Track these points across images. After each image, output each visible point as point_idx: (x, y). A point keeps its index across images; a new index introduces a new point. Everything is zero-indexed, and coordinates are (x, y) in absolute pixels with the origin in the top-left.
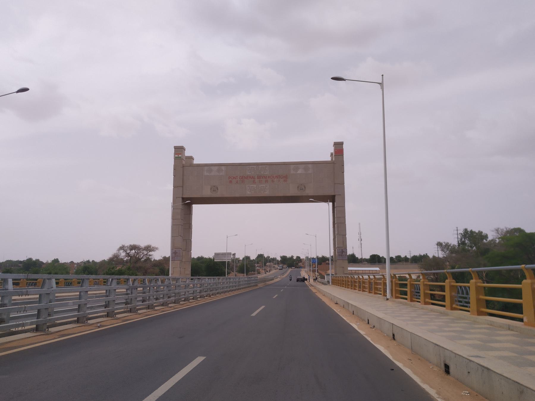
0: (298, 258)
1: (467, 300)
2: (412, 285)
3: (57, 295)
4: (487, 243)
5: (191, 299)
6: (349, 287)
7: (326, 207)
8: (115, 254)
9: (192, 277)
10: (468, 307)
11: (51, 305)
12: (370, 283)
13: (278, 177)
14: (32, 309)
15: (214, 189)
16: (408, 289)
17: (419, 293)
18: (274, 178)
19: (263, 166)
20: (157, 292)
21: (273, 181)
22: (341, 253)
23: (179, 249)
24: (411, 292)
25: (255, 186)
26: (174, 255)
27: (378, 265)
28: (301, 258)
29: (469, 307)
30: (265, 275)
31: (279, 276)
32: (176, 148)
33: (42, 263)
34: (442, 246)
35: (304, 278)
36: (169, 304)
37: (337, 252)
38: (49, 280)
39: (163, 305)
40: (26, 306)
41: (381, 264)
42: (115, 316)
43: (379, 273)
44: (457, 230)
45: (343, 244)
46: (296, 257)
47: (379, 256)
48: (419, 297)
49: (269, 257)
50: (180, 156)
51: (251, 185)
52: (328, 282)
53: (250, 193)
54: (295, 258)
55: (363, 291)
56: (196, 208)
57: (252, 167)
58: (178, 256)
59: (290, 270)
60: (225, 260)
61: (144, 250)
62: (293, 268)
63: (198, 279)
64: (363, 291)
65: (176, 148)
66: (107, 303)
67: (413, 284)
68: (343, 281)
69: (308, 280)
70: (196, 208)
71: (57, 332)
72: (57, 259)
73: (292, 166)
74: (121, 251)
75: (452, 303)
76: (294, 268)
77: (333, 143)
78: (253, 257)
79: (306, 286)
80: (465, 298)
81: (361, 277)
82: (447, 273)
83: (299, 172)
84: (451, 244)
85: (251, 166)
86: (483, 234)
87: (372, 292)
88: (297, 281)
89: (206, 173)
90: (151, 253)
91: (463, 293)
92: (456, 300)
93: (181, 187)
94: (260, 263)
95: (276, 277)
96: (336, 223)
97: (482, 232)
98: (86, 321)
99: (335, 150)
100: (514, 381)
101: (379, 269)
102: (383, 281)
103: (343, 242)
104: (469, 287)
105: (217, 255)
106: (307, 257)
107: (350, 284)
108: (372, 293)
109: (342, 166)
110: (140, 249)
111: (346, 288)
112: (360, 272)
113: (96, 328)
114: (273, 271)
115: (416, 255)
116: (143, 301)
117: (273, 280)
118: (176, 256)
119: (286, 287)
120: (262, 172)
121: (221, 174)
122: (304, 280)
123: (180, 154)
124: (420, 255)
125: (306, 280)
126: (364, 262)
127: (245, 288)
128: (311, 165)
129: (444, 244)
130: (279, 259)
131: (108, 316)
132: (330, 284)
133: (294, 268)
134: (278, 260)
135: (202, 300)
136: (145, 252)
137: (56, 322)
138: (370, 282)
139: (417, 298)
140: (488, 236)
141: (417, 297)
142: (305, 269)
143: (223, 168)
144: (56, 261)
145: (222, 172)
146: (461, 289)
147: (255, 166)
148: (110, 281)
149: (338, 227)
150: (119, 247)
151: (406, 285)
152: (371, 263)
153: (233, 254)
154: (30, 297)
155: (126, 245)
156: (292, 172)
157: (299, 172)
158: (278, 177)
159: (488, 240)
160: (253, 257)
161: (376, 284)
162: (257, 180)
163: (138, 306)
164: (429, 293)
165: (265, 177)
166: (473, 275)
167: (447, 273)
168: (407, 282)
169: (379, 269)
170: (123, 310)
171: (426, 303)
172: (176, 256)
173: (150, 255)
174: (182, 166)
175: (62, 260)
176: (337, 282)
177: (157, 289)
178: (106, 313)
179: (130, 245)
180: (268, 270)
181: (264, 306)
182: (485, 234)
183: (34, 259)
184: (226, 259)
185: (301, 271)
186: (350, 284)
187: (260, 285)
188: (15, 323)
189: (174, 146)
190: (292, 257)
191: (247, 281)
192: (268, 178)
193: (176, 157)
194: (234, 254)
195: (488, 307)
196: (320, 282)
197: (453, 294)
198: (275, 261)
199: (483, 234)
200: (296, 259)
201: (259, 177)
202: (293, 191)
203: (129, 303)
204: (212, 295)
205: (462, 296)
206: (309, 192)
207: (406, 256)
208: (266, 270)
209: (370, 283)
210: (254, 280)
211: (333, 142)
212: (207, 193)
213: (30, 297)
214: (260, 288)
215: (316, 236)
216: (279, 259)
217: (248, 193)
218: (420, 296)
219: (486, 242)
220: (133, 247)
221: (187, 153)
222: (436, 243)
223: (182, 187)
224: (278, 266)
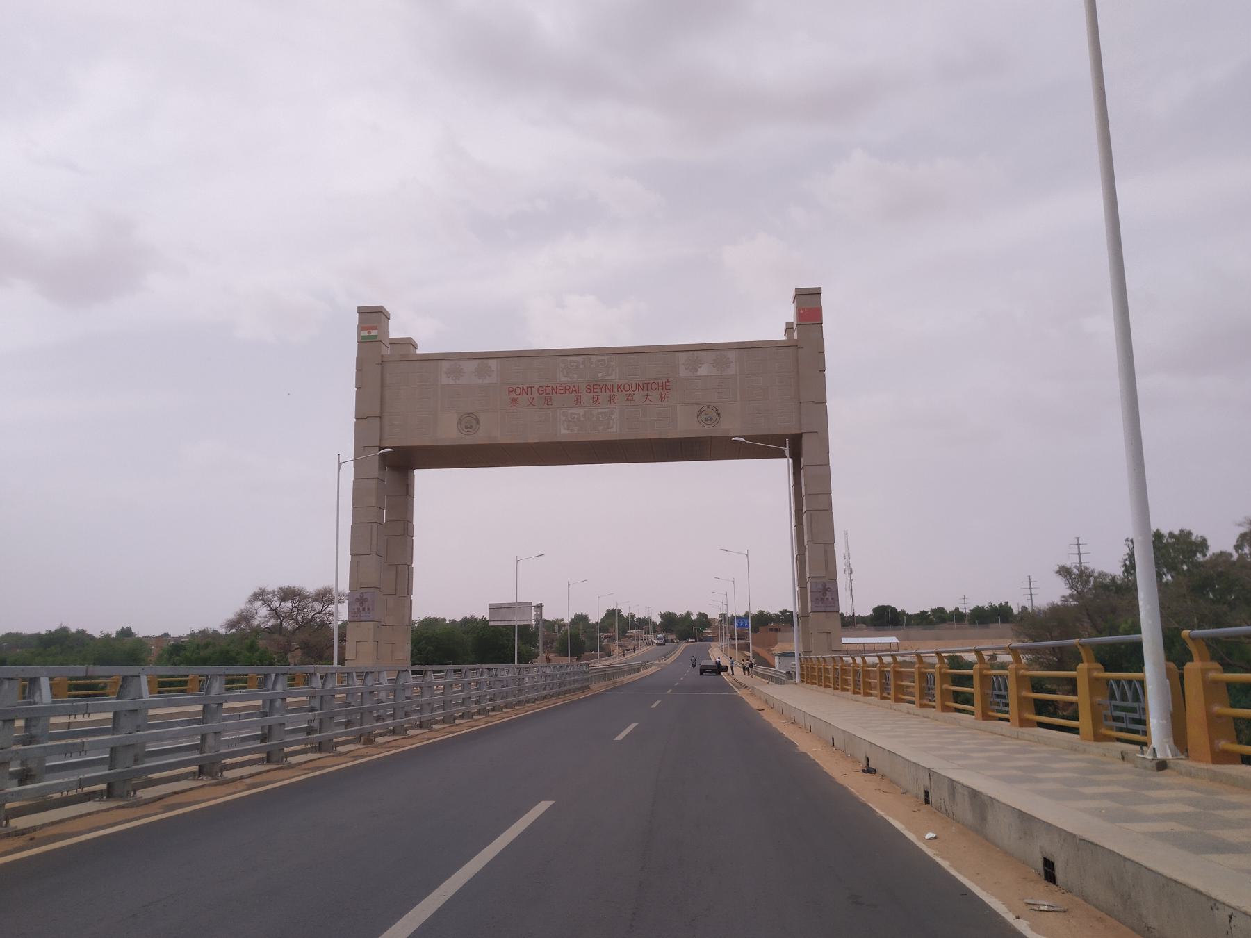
0: (703, 616)
1: (1136, 716)
2: (984, 677)
3: (151, 712)
4: (1206, 562)
5: (438, 722)
6: (814, 681)
7: (780, 468)
8: (241, 610)
9: (417, 668)
10: (1141, 732)
11: (226, 725)
12: (883, 674)
13: (645, 385)
14: (95, 747)
15: (469, 421)
16: (975, 690)
17: (1004, 697)
18: (634, 389)
19: (603, 357)
20: (28, 740)
21: (630, 398)
22: (821, 593)
23: (372, 590)
24: (984, 695)
25: (581, 412)
26: (357, 606)
27: (895, 630)
28: (709, 618)
29: (934, 701)
30: (622, 658)
31: (657, 662)
32: (362, 312)
33: (91, 637)
34: (1071, 576)
35: (718, 663)
36: (488, 711)
37: (811, 592)
38: (12, 681)
39: (393, 732)
40: (85, 740)
41: (902, 627)
42: (284, 759)
43: (898, 651)
44: (1078, 545)
45: (827, 568)
46: (698, 615)
47: (894, 610)
48: (1006, 709)
49: (633, 616)
50: (374, 333)
51: (570, 411)
52: (790, 675)
53: (566, 432)
54: (694, 617)
55: (825, 687)
56: (424, 479)
57: (571, 361)
58: (369, 609)
59: (684, 645)
60: (512, 623)
61: (316, 600)
62: (690, 640)
63: (455, 671)
64: (866, 694)
65: (362, 312)
66: (266, 731)
67: (986, 676)
68: (827, 670)
69: (729, 671)
70: (424, 479)
71: (250, 777)
72: (129, 629)
73: (682, 357)
74: (258, 604)
75: (1096, 722)
76: (694, 640)
77: (792, 293)
78: (595, 617)
79: (725, 687)
80: (1133, 710)
81: (859, 660)
82: (1079, 646)
83: (703, 371)
84: (1093, 572)
85: (569, 359)
86: (1193, 538)
87: (933, 704)
88: (701, 674)
89: (445, 380)
90: (331, 608)
91: (1124, 698)
92: (1105, 716)
93: (378, 419)
94: (611, 630)
95: (646, 663)
96: (804, 510)
97: (1190, 534)
98: (132, 793)
99: (798, 310)
100: (1014, 808)
101: (898, 641)
102: (919, 668)
103: (826, 562)
104: (1007, 676)
105: (494, 608)
106: (724, 616)
107: (816, 674)
108: (889, 699)
109: (820, 352)
110: (306, 597)
111: (837, 689)
112: (851, 647)
113: (310, 771)
114: (644, 649)
115: (980, 605)
116: (347, 724)
117: (638, 670)
118: (364, 609)
119: (669, 692)
120: (600, 375)
121: (486, 381)
122: (718, 669)
123: (375, 328)
124: (991, 606)
125: (725, 669)
126: (858, 625)
127: (574, 690)
128: (733, 352)
129: (1075, 571)
130: (657, 620)
131: (268, 760)
132: (798, 680)
133: (694, 640)
134: (654, 623)
135: (466, 725)
136: (318, 606)
137: (52, 797)
138: (856, 670)
139: (998, 711)
140: (1209, 543)
141: (1119, 724)
142: (721, 644)
143: (493, 364)
144: (126, 633)
145: (489, 376)
146: (1118, 686)
147: (580, 359)
148: (273, 678)
149: (811, 522)
150: (253, 593)
151: (970, 677)
152: (875, 625)
153: (537, 607)
154: (94, 717)
155: (269, 589)
156: (683, 372)
157: (703, 371)
158: (645, 385)
159: (1209, 554)
160: (595, 617)
161: (899, 675)
162: (586, 397)
163: (337, 736)
164: (1031, 698)
165: (609, 388)
166: (1083, 654)
167: (1079, 646)
168: (971, 671)
169: (898, 641)
170: (302, 746)
171: (1024, 723)
172: (364, 609)
173: (331, 614)
174: (380, 362)
175: (141, 631)
176: (814, 675)
177: (27, 727)
178: (265, 755)
179: (281, 589)
180: (630, 647)
181: (616, 739)
182: (1199, 539)
183: (73, 630)
184: (516, 620)
185: (710, 647)
186: (816, 674)
187: (597, 687)
188: (61, 781)
189: (358, 308)
190: (689, 614)
191: (553, 676)
192: (615, 389)
193: (363, 337)
194: (539, 607)
195: (1039, 713)
196: (763, 676)
197: (1099, 699)
198: (648, 624)
199: (1193, 538)
200: (698, 618)
201: (592, 388)
202: (685, 426)
203: (316, 730)
204: (493, 710)
205: (1124, 704)
206: (733, 426)
207: (957, 609)
208: (626, 647)
209: (883, 674)
210: (574, 674)
211: (794, 290)
212: (448, 433)
213: (94, 717)
214: (595, 696)
215: (747, 555)
216: (657, 620)
217: (564, 431)
218: (1007, 705)
219: (1205, 559)
220: (288, 594)
221: (395, 331)
222: (1057, 568)
223: (380, 417)
224: (655, 637)
